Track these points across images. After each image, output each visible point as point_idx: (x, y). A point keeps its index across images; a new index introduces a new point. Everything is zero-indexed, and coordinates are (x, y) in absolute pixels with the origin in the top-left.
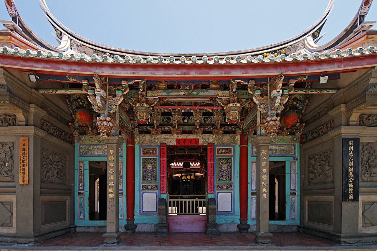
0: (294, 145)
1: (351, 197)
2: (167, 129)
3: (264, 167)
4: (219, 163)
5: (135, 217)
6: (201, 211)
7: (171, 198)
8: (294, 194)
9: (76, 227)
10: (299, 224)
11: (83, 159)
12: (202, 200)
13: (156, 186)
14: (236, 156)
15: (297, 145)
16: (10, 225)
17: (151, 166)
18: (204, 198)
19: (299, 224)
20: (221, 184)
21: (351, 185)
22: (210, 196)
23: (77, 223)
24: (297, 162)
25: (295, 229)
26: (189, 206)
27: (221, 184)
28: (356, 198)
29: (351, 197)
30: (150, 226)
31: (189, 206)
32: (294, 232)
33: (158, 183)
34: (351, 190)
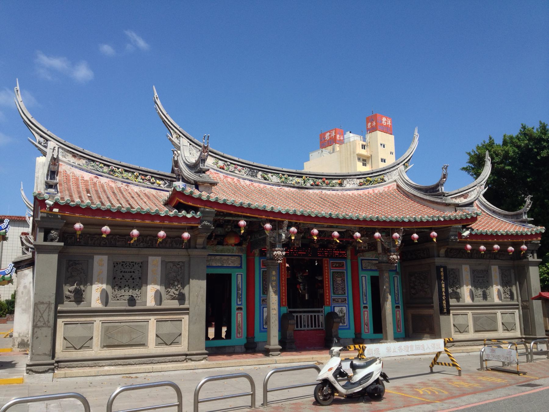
1: (445, 311)
12: (320, 314)
28: (448, 313)
29: (445, 311)
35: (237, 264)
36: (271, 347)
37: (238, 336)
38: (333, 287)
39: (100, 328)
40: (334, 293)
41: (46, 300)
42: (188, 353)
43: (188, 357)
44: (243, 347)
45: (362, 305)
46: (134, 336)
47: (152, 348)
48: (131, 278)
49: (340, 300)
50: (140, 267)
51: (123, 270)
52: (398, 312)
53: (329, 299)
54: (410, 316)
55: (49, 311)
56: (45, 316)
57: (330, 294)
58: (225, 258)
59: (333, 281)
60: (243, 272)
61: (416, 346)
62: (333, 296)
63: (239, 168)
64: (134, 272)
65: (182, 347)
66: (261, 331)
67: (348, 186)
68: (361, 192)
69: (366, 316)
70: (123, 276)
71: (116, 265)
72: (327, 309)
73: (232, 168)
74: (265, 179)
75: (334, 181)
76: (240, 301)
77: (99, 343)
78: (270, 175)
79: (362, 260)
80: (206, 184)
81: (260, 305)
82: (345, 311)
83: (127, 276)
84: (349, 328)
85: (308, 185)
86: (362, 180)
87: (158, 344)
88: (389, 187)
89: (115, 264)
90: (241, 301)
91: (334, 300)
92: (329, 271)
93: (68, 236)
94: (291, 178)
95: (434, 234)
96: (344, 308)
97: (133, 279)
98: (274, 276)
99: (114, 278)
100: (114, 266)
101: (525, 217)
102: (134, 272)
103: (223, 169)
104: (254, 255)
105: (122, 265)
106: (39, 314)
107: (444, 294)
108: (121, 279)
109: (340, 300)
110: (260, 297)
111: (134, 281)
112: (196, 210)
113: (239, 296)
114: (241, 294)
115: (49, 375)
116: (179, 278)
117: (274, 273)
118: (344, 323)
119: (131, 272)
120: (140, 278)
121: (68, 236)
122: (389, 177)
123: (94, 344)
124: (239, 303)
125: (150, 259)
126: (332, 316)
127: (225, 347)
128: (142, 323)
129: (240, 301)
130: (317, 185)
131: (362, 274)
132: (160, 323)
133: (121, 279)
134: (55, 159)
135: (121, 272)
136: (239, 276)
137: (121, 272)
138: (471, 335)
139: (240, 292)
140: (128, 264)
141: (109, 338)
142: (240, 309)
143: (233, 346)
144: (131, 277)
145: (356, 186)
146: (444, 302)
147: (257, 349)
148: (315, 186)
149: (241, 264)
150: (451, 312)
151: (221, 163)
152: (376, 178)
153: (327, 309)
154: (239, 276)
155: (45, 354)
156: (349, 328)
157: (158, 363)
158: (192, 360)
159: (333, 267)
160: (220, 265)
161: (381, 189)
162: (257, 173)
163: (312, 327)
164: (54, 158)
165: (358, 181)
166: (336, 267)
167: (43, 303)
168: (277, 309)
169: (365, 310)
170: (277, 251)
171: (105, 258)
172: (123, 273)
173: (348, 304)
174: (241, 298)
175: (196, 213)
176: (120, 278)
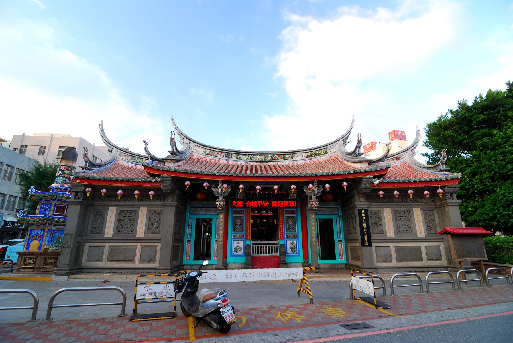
0: (338, 208)
1: (367, 243)
2: (251, 197)
3: (313, 226)
4: (286, 219)
5: (227, 258)
6: (140, 232)
7: (253, 244)
8: (341, 241)
9: (183, 265)
10: (346, 263)
11: (191, 217)
12: (276, 245)
13: (243, 236)
14: (237, 270)
15: (340, 208)
16: (154, 261)
17: (239, 221)
18: (277, 244)
19: (346, 263)
20: (289, 234)
21: (366, 237)
22: (281, 242)
23: (184, 263)
24: (341, 219)
25: (343, 266)
26: (264, 250)
27: (289, 234)
28: (370, 245)
29: (367, 243)
30: (238, 265)
31: (264, 250)
32: (343, 269)
33: (244, 233)
34: (366, 239)
41: (71, 232)
47: (137, 264)
49: (291, 236)
52: (340, 245)
54: (349, 248)
56: (69, 242)
58: (209, 209)
59: (287, 222)
61: (265, 273)
63: (220, 153)
65: (155, 265)
66: (231, 256)
67: (298, 158)
68: (308, 162)
73: (215, 153)
74: (238, 159)
75: (287, 156)
78: (240, 155)
81: (231, 239)
82: (295, 244)
83: (127, 219)
84: (299, 256)
85: (268, 160)
86: (309, 154)
87: (429, 260)
88: (331, 157)
94: (255, 156)
95: (345, 184)
96: (295, 242)
101: (442, 167)
103: (210, 155)
106: (66, 241)
109: (291, 236)
110: (232, 234)
112: (159, 176)
115: (66, 277)
116: (157, 220)
117: (222, 216)
118: (295, 252)
122: (331, 150)
130: (275, 159)
138: (394, 263)
145: (304, 158)
147: (228, 268)
148: (273, 159)
150: (373, 244)
151: (208, 151)
152: (320, 152)
155: (66, 264)
156: (299, 256)
159: (286, 213)
161: (324, 158)
162: (232, 155)
163: (269, 254)
165: (306, 154)
166: (288, 213)
167: (68, 234)
171: (115, 209)
173: (298, 239)
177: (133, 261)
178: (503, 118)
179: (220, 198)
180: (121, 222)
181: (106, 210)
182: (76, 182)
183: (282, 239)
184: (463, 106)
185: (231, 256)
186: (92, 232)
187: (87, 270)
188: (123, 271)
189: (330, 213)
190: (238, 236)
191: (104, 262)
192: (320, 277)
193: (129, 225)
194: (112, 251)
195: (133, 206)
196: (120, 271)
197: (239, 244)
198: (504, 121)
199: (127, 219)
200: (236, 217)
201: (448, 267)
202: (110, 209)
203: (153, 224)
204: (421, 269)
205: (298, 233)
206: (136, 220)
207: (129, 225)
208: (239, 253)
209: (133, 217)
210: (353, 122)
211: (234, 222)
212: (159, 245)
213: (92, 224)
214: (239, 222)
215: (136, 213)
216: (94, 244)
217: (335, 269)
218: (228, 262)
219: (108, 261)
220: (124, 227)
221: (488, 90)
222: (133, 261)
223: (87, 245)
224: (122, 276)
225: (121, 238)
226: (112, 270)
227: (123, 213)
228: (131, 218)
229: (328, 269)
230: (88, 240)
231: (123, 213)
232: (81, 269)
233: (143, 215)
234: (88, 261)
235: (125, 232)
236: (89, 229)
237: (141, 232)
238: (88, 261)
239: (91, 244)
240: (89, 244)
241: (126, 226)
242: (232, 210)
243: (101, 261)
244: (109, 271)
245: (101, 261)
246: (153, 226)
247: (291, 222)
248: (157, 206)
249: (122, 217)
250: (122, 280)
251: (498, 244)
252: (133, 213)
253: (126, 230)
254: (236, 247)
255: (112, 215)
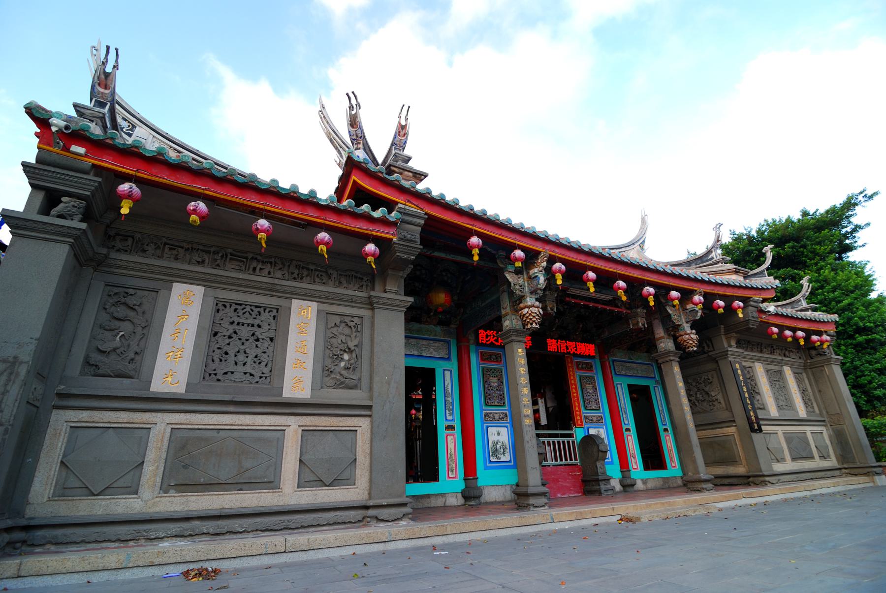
18: (571, 436)
35: (443, 354)
36: (531, 490)
37: (451, 476)
38: (584, 399)
39: (166, 443)
40: (586, 408)
42: (371, 503)
43: (371, 512)
44: (460, 495)
45: (624, 427)
46: (247, 464)
47: (289, 493)
48: (252, 339)
49: (595, 419)
50: (274, 317)
51: (236, 320)
53: (580, 415)
55: (9, 380)
57: (581, 411)
58: (424, 342)
59: (582, 389)
60: (454, 365)
62: (585, 413)
64: (259, 326)
65: (354, 493)
66: (486, 468)
69: (630, 444)
70: (235, 333)
71: (221, 308)
72: (579, 434)
76: (450, 414)
77: (159, 480)
79: (614, 361)
80: (407, 173)
81: (482, 424)
83: (244, 332)
87: (302, 484)
89: (220, 306)
90: (452, 414)
91: (586, 418)
92: (575, 377)
93: (99, 208)
96: (601, 430)
97: (257, 340)
98: (521, 357)
99: (215, 334)
100: (218, 311)
102: (259, 326)
104: (468, 341)
105: (235, 310)
107: (750, 407)
108: (230, 337)
109: (595, 419)
110: (481, 410)
111: (259, 343)
112: (390, 206)
113: (448, 406)
114: (452, 403)
119: (253, 326)
120: (271, 339)
121: (99, 208)
123: (143, 480)
124: (448, 418)
125: (296, 303)
126: (590, 441)
127: (428, 496)
128: (268, 434)
129: (450, 414)
131: (617, 380)
132: (305, 433)
133: (230, 337)
134: (107, 75)
135: (232, 323)
136: (447, 374)
137: (232, 323)
139: (450, 399)
140: (248, 308)
141: (185, 467)
142: (450, 428)
143: (443, 495)
144: (253, 335)
146: (752, 414)
149: (449, 354)
153: (579, 434)
154: (447, 374)
157: (303, 527)
158: (379, 520)
159: (578, 369)
160: (416, 353)
164: (105, 73)
166: (582, 369)
168: (532, 416)
169: (628, 433)
170: (529, 307)
171: (198, 291)
172: (235, 326)
173: (606, 425)
174: (453, 409)
175: (390, 212)
176: (228, 334)
177: (272, 484)
178: (810, 255)
179: (530, 300)
180: (223, 342)
181: (158, 290)
182: (66, 149)
183: (581, 425)
184: (835, 207)
185: (486, 468)
186: (91, 367)
187: (59, 532)
188: (236, 524)
189: (644, 374)
190: (497, 416)
191: (146, 492)
192: (737, 498)
193: (252, 353)
194: (182, 446)
195: (271, 290)
196: (221, 523)
197: (500, 435)
198: (811, 260)
199: (244, 332)
200: (489, 370)
201: (840, 469)
202: (179, 290)
203: (338, 358)
204: (829, 473)
205: (603, 413)
206: (278, 338)
207: (252, 353)
208: (503, 459)
209: (265, 327)
210: (644, 221)
211: (485, 382)
212: (363, 425)
213: (93, 337)
214: (494, 382)
215: (280, 316)
216: (97, 416)
217: (669, 487)
218: (480, 483)
219: (165, 488)
220: (231, 358)
221: (820, 204)
222: (272, 484)
223: (61, 422)
224: (264, 540)
225: (227, 398)
226: (184, 524)
227: (230, 311)
228: (258, 332)
229: (655, 489)
230: (67, 399)
231: (230, 311)
232: (27, 528)
233: (303, 323)
234: (63, 491)
235: (238, 376)
236: (79, 353)
237: (298, 378)
238: (63, 491)
239: (84, 415)
240: (72, 415)
241: (241, 357)
242: (477, 351)
243: (134, 490)
244: (175, 527)
245: (134, 490)
246: (339, 359)
247: (589, 387)
248: (350, 301)
249: (225, 323)
250: (266, 560)
251: (873, 430)
252: (265, 316)
253: (240, 368)
254: (496, 443)
255: (183, 315)
